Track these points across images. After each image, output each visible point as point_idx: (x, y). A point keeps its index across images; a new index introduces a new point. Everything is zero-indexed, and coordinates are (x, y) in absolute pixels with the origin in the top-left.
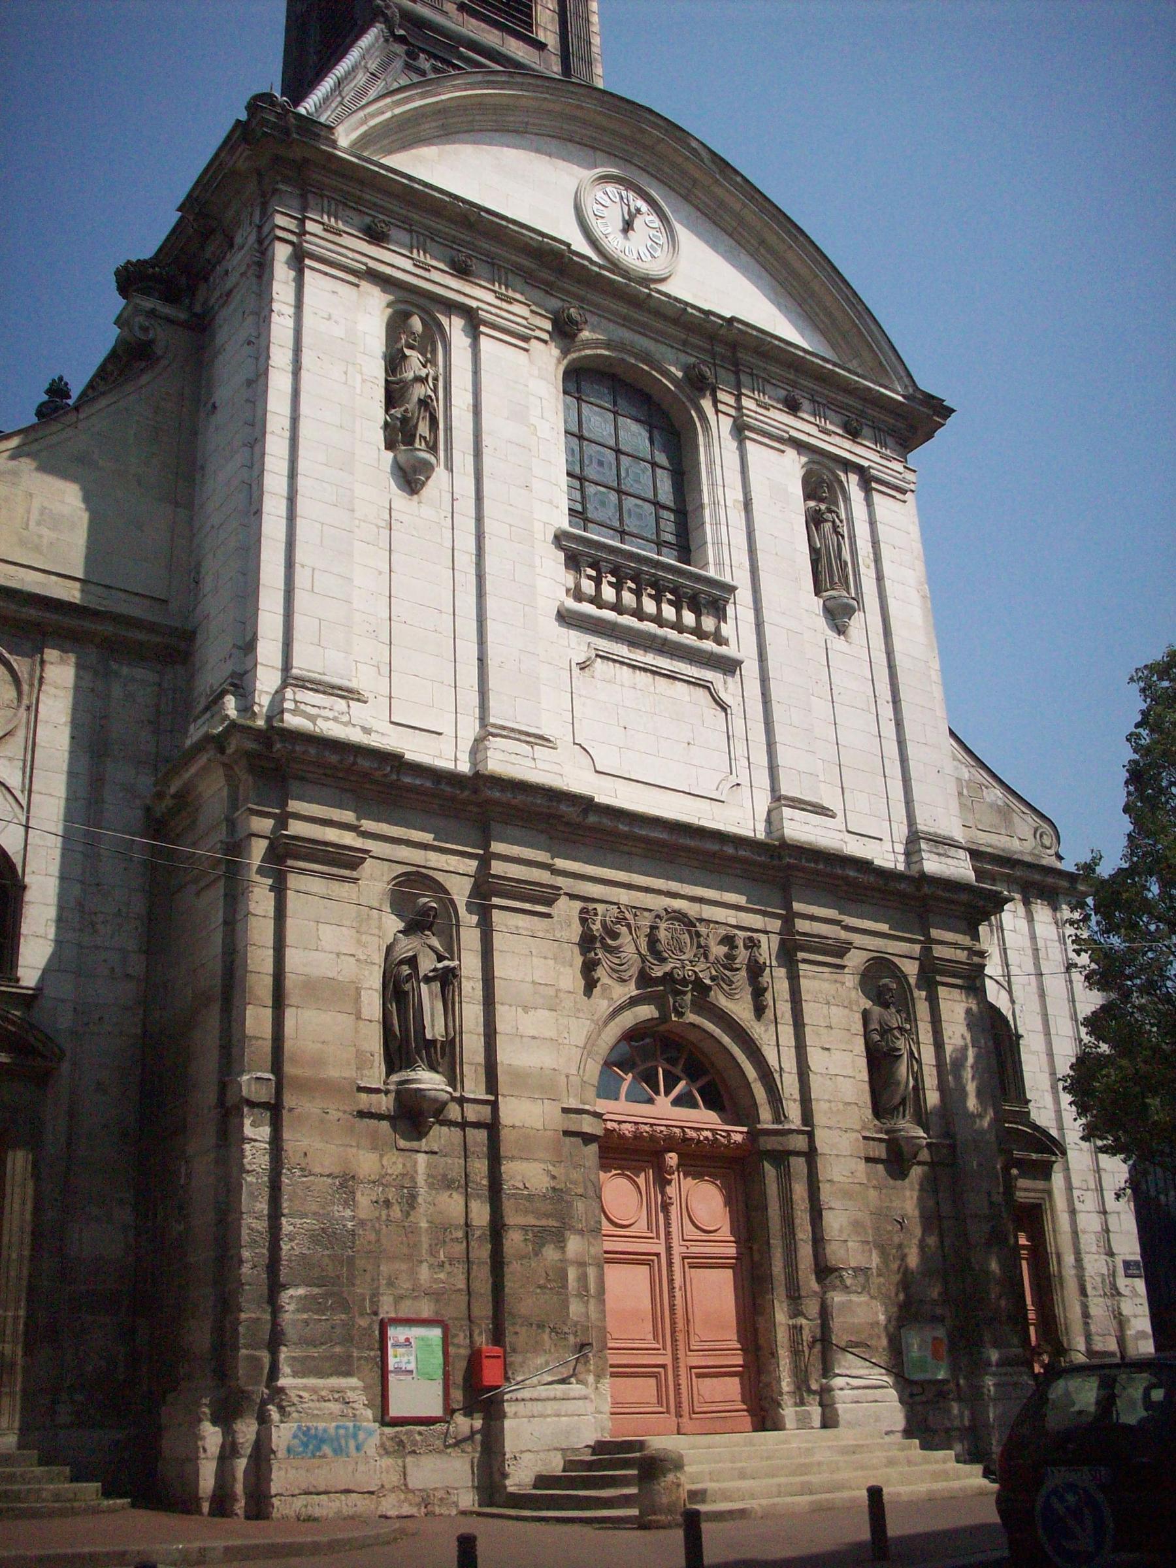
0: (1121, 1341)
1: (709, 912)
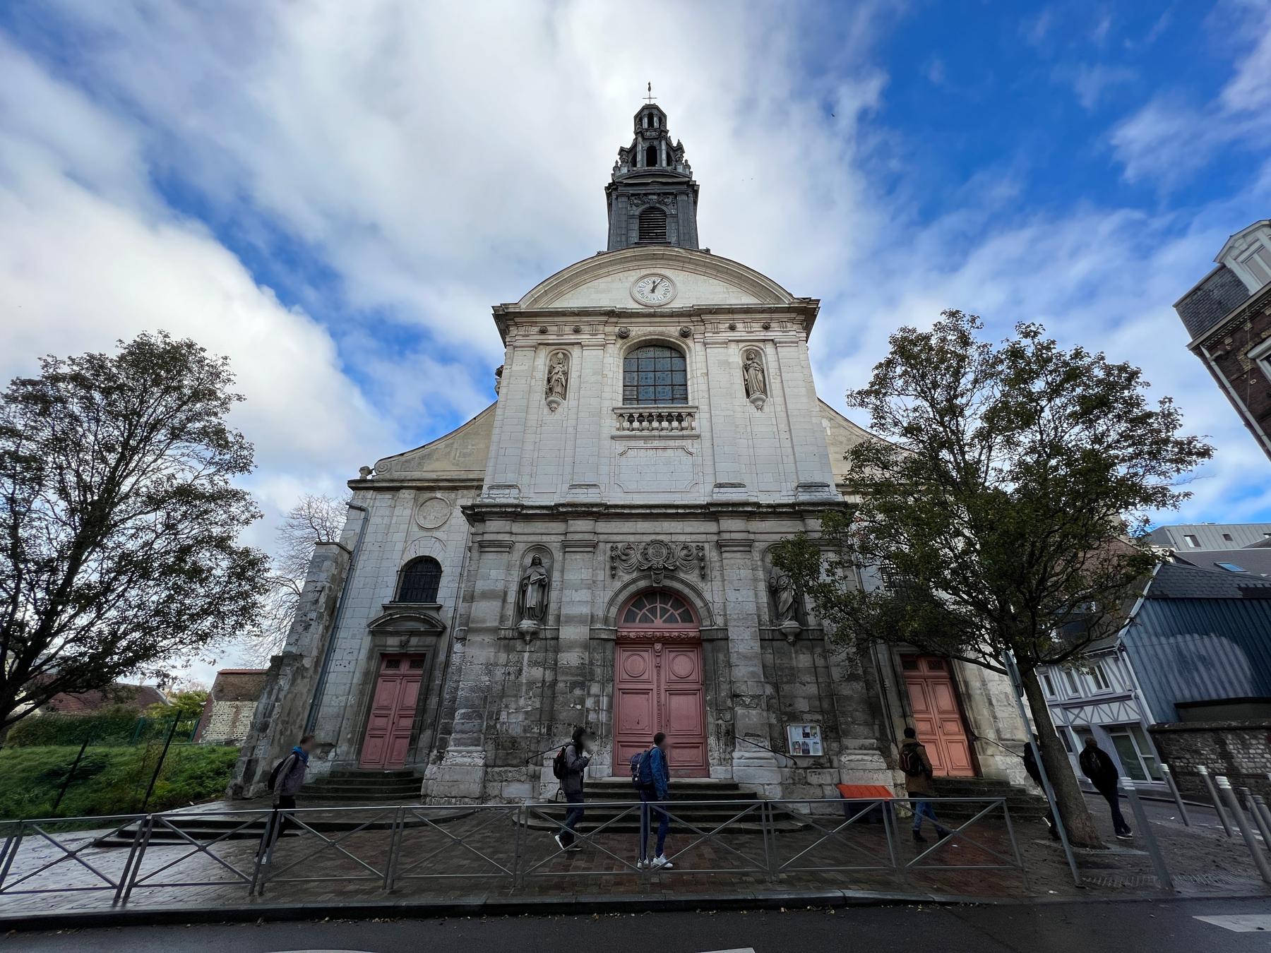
0: (1201, 697)
1: (675, 538)
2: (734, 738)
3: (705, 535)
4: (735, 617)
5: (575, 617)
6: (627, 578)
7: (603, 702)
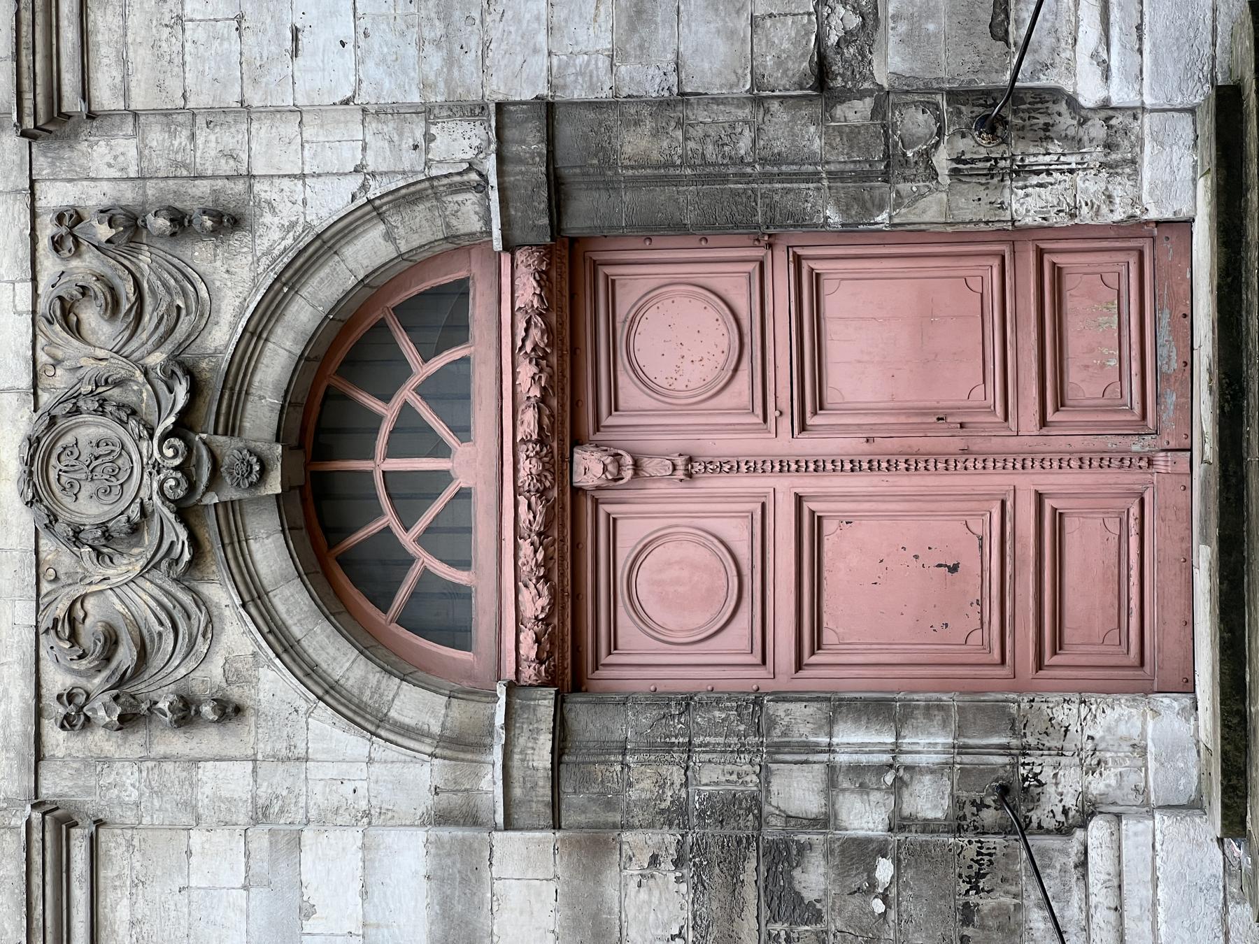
2: (1013, 94)
4: (436, 60)
5: (445, 904)
7: (861, 748)
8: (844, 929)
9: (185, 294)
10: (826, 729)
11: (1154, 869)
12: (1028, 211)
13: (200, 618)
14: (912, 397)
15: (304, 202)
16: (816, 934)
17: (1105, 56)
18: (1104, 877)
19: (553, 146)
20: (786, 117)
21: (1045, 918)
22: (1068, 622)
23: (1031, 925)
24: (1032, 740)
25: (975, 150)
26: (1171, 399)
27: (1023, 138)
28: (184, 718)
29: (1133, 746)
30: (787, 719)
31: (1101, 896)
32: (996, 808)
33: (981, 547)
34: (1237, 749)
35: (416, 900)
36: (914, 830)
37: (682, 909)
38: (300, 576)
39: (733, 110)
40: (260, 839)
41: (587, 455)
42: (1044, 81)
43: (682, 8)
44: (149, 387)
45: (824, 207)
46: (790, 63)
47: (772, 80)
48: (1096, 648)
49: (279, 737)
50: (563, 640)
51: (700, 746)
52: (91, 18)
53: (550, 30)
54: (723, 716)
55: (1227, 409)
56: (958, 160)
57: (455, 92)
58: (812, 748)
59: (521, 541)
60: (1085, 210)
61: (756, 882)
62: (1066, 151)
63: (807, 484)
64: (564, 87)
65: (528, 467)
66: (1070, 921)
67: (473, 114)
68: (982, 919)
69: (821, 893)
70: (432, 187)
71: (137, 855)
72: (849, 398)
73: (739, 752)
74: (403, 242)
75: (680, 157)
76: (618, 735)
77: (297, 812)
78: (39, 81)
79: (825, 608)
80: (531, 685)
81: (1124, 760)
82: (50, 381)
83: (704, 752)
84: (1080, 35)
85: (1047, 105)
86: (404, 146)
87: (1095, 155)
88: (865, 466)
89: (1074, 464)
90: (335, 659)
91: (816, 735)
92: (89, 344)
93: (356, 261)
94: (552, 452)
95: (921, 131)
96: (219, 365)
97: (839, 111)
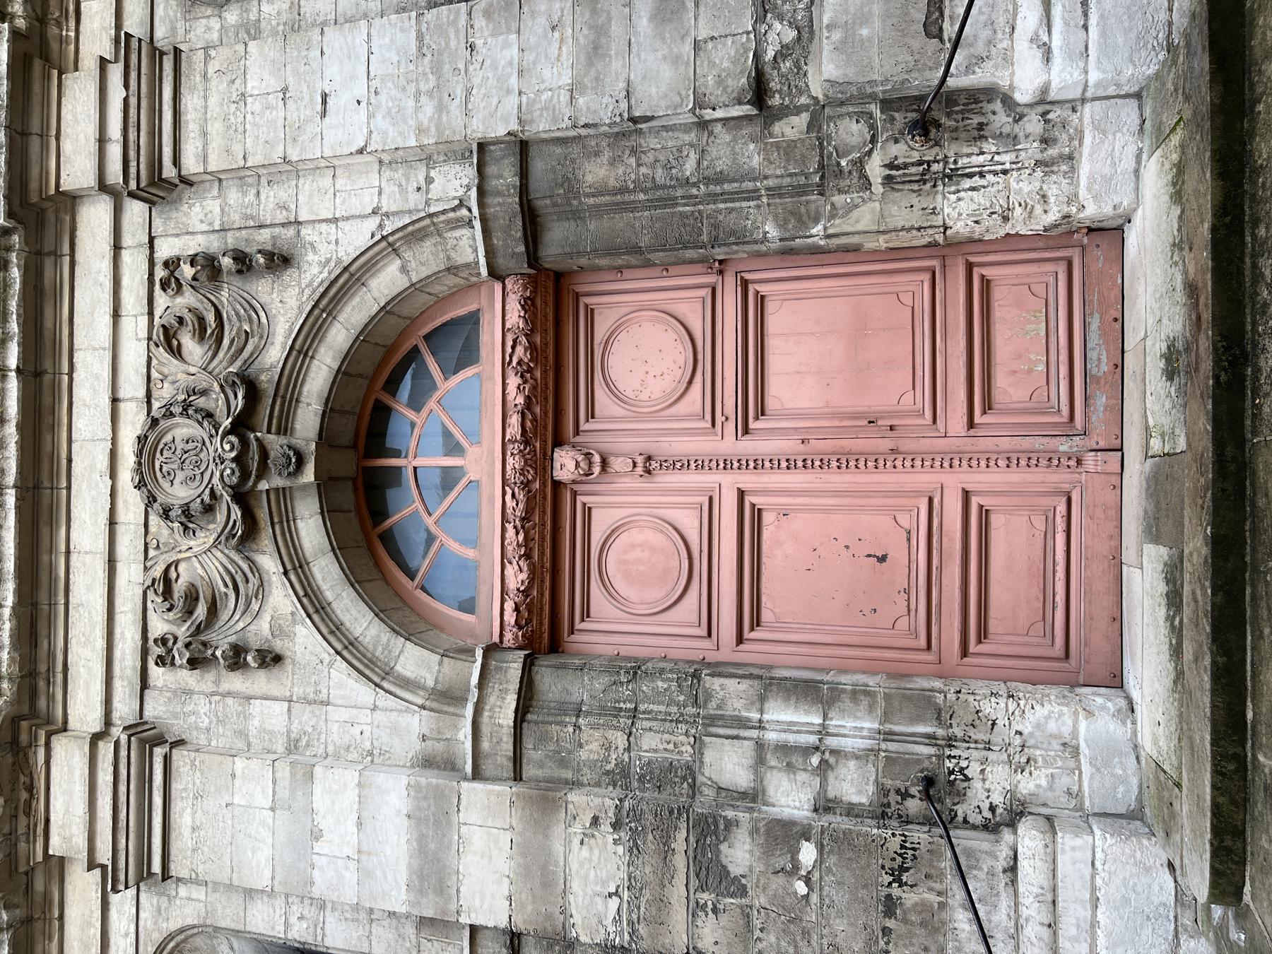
1: (132, 387)
2: (945, 97)
3: (126, 256)
4: (429, 108)
5: (422, 841)
6: (281, 599)
7: (789, 727)
8: (768, 907)
9: (250, 320)
10: (758, 705)
11: (1094, 888)
12: (960, 214)
13: (254, 581)
14: (844, 401)
15: (337, 242)
16: (741, 908)
17: (1045, 39)
18: (1036, 890)
19: (527, 179)
20: (728, 138)
21: (970, 920)
22: (993, 612)
23: (956, 925)
24: (958, 732)
25: (908, 154)
26: (1101, 401)
27: (957, 139)
28: (236, 664)
29: (1064, 744)
30: (722, 693)
31: (1032, 910)
32: (920, 799)
33: (909, 540)
34: (1233, 802)
35: (399, 834)
36: (838, 812)
37: (619, 869)
38: (333, 549)
39: (680, 135)
40: (284, 771)
41: (563, 453)
42: (978, 78)
43: (633, 40)
44: (222, 395)
45: (764, 223)
46: (730, 80)
47: (712, 98)
48: (1020, 639)
49: (309, 683)
50: (541, 609)
51: (644, 713)
52: (183, 102)
53: (521, 72)
54: (665, 686)
55: (1223, 377)
56: (891, 166)
57: (443, 134)
58: (743, 723)
59: (507, 525)
60: (1018, 210)
61: (686, 852)
62: (1001, 150)
63: (747, 480)
64: (532, 121)
65: (514, 462)
66: (997, 926)
67: (463, 157)
68: (904, 912)
69: (747, 869)
70: (434, 224)
71: (198, 773)
72: (788, 405)
73: (677, 722)
74: (414, 273)
75: (634, 182)
76: (575, 698)
77: (319, 747)
78: (142, 152)
79: (764, 590)
80: (509, 648)
81: (1055, 760)
82: (159, 392)
83: (647, 719)
84: (1019, 22)
85: (980, 105)
86: (410, 189)
87: (1031, 150)
88: (800, 464)
89: (1002, 463)
90: (356, 619)
91: (748, 710)
92: (185, 362)
93: (379, 291)
94: (535, 451)
95: (855, 140)
96: (272, 377)
97: (777, 127)
